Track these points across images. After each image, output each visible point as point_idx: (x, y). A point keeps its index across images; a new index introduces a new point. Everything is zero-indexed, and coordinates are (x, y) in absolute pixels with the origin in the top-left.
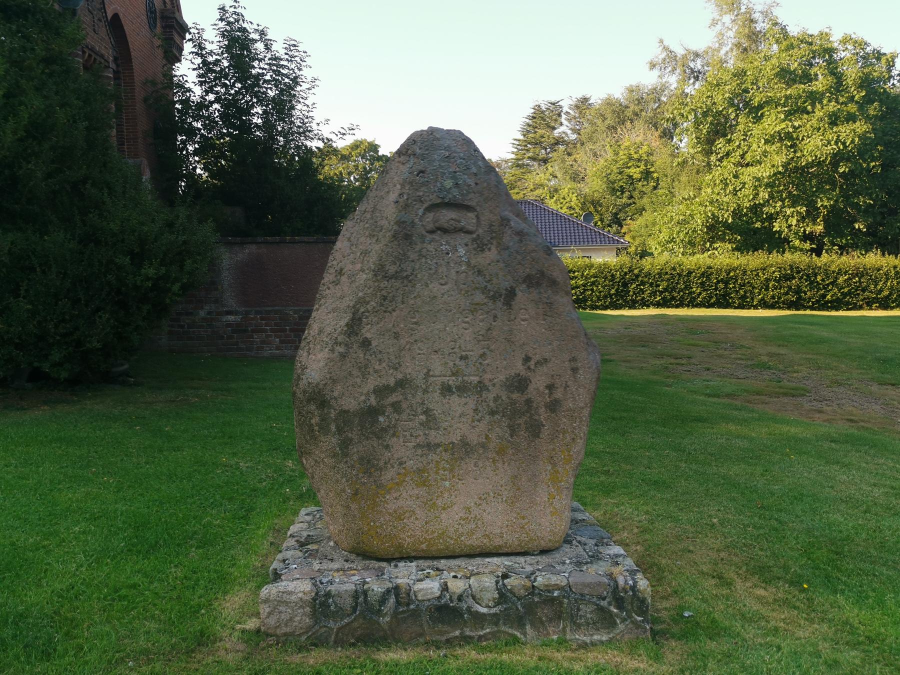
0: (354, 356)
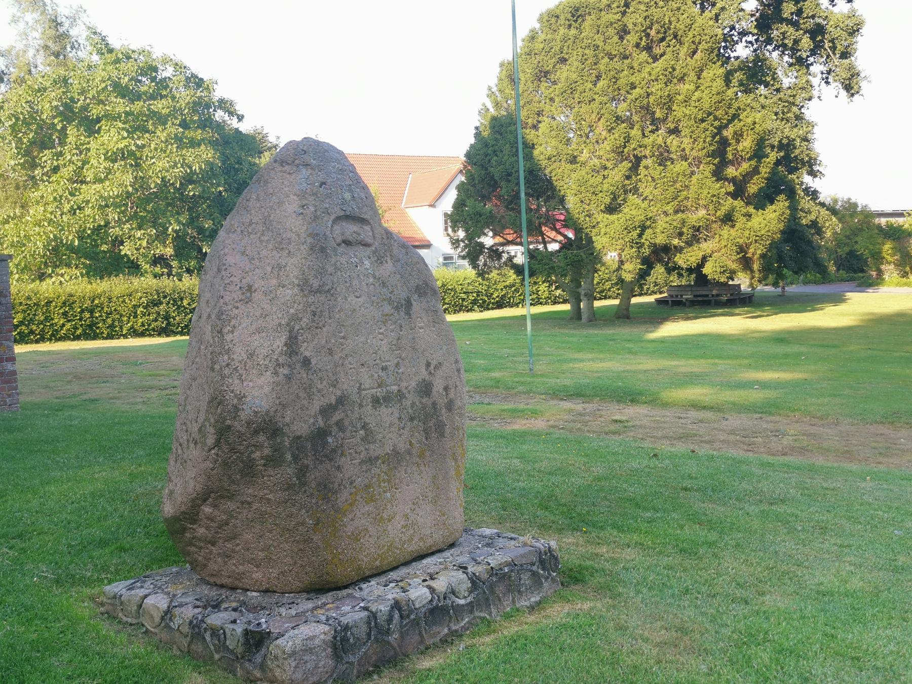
0: (299, 376)
